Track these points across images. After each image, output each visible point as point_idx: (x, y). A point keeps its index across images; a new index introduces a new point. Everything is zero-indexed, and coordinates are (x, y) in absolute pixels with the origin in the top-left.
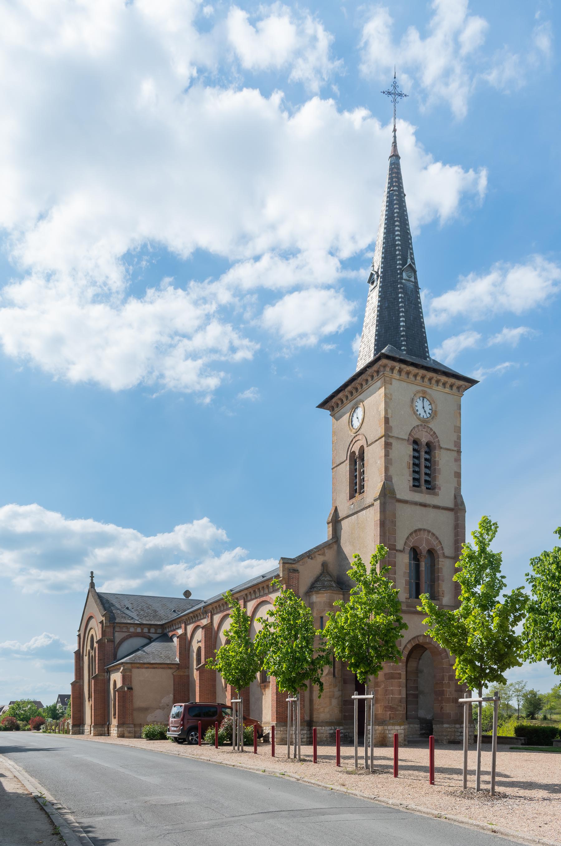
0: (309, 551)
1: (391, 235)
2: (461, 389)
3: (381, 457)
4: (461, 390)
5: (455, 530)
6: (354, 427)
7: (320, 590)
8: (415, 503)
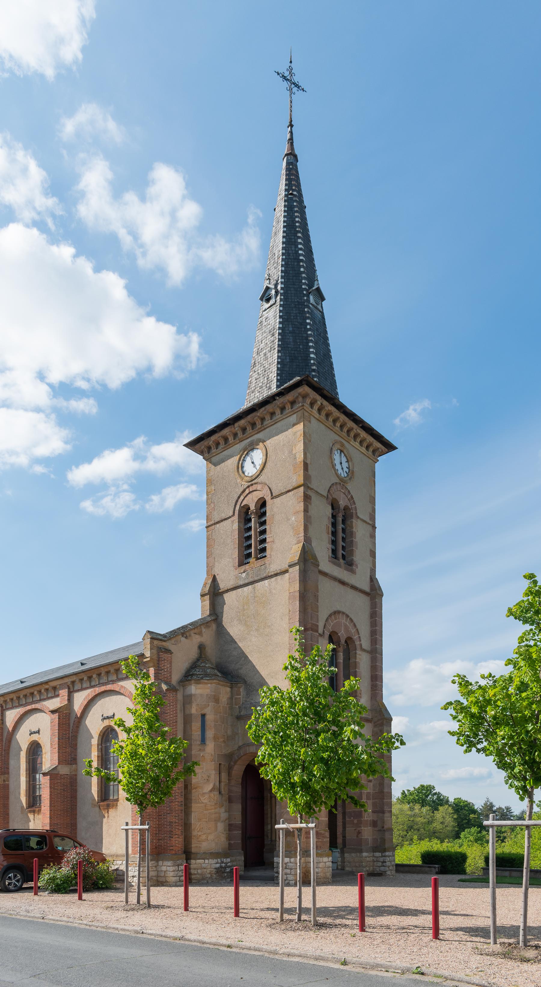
0: (183, 627)
1: (293, 246)
2: (377, 454)
3: (298, 512)
4: (377, 453)
5: (371, 619)
6: (246, 474)
7: (202, 678)
8: (335, 579)
